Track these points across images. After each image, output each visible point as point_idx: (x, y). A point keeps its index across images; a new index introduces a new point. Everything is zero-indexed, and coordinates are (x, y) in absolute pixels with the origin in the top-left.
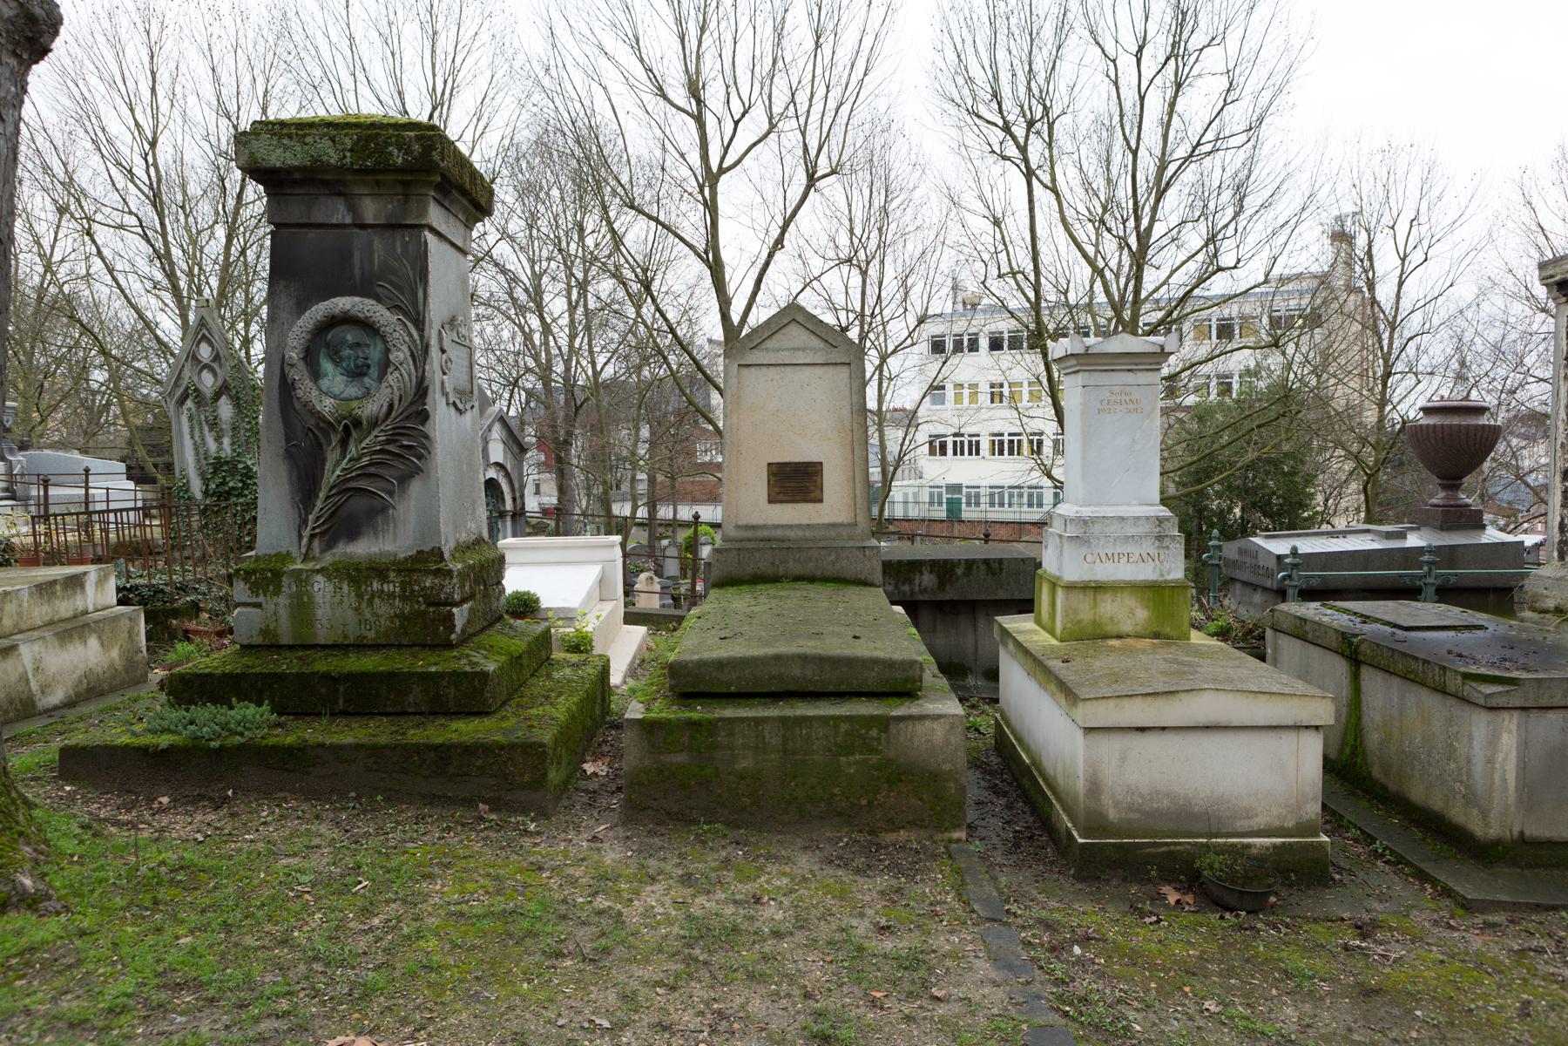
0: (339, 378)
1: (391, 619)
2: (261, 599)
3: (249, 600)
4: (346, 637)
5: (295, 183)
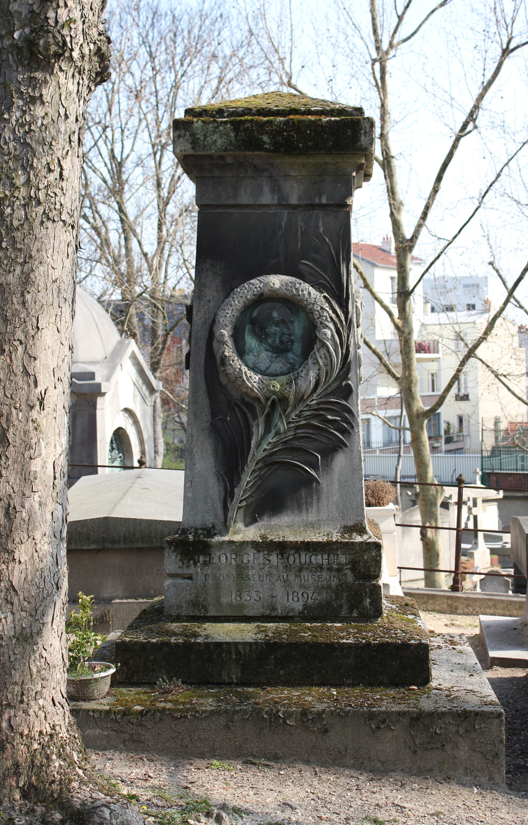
0: (264, 355)
2: (191, 570)
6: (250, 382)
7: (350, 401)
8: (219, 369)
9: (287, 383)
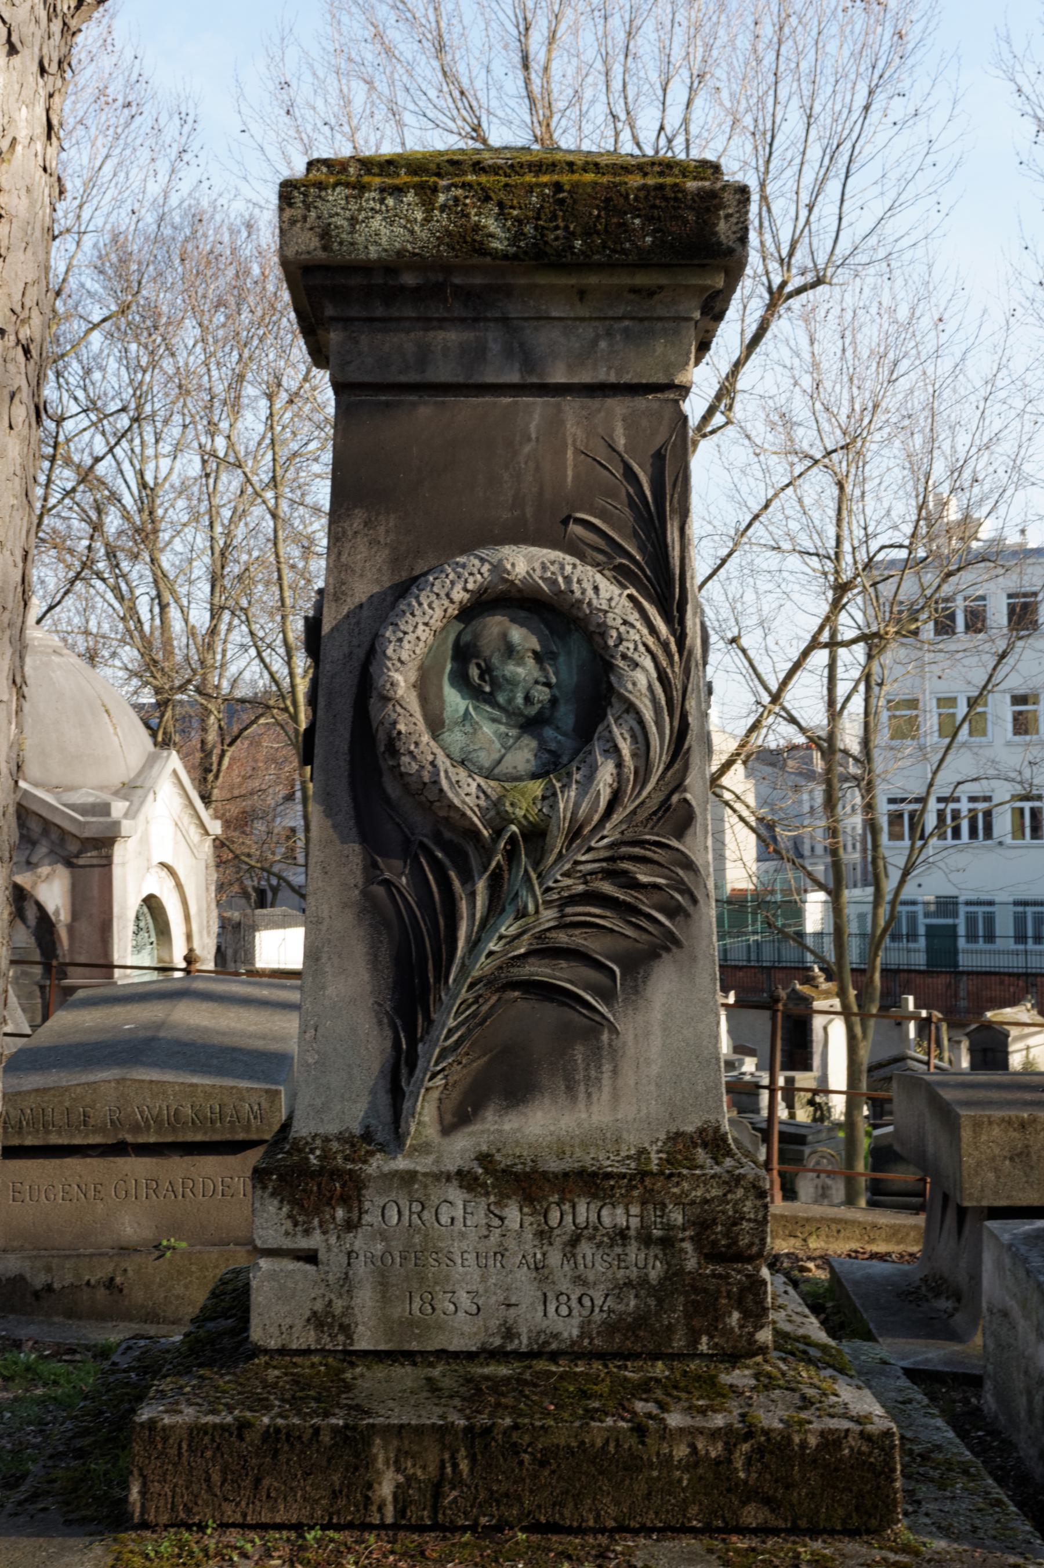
1: (620, 1289)
2: (315, 1241)
3: (287, 1243)
4: (509, 1333)
5: (393, 294)
6: (457, 794)
7: (688, 838)
8: (381, 762)
9: (544, 798)
